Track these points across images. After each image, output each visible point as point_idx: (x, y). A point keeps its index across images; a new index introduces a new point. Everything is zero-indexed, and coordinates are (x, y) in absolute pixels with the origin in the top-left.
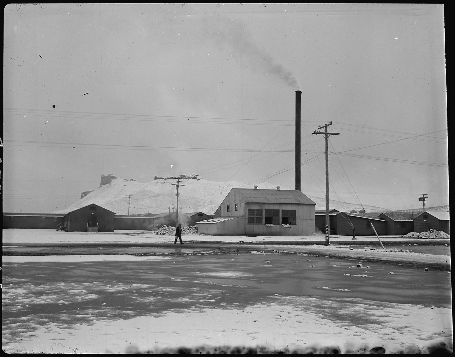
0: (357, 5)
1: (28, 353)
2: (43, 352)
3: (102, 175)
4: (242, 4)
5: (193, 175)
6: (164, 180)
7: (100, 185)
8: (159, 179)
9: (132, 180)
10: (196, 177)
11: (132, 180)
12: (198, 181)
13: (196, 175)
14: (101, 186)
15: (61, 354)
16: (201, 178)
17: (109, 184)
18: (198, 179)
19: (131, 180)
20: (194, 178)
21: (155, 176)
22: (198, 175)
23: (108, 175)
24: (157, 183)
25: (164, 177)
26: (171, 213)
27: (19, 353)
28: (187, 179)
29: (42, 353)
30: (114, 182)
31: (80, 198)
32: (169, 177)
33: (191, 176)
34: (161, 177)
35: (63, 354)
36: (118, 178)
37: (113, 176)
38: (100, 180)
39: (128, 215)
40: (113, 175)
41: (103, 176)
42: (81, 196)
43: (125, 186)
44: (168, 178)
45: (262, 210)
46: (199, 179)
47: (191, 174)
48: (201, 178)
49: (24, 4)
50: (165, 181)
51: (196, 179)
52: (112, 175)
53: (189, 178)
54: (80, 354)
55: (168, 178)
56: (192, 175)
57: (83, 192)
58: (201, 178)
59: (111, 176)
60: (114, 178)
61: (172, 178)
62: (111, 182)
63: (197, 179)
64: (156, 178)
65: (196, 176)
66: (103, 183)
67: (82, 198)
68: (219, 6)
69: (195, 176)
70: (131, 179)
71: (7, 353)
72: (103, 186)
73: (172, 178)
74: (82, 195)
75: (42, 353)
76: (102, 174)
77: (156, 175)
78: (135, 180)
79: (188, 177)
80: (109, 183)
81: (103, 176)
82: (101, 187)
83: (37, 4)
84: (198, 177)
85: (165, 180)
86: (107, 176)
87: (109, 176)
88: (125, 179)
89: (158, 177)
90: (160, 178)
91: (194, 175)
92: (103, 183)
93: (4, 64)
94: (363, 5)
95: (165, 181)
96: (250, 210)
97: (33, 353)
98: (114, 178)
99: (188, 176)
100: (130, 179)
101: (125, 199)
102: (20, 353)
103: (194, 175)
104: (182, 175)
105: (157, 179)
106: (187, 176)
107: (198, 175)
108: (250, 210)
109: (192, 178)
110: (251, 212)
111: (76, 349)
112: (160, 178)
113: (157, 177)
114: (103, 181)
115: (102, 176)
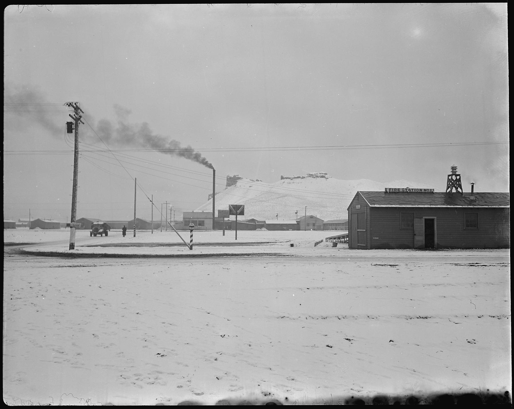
0: (408, 4)
1: (34, 405)
2: (50, 404)
3: (227, 176)
4: (277, 4)
5: (321, 173)
6: (290, 179)
7: (226, 186)
8: (285, 179)
9: (257, 180)
10: (324, 176)
11: (258, 181)
12: (326, 180)
13: (324, 174)
14: (227, 187)
15: (72, 406)
16: (330, 177)
17: (234, 186)
18: (326, 177)
19: (256, 181)
20: (322, 177)
21: (281, 176)
22: (326, 174)
23: (233, 175)
24: (283, 183)
25: (290, 177)
26: (154, 222)
27: (23, 405)
28: (315, 178)
29: (50, 404)
30: (239, 183)
31: (208, 200)
32: (296, 176)
33: (319, 175)
34: (287, 177)
35: (74, 406)
36: (244, 179)
37: (238, 176)
38: (225, 182)
39: (212, 219)
40: (238, 175)
41: (228, 177)
42: (208, 198)
43: (250, 187)
44: (295, 178)
45: (190, 221)
46: (328, 177)
47: (319, 173)
48: (329, 176)
49: (27, 5)
50: (292, 181)
51: (324, 178)
52: (237, 176)
53: (318, 177)
54: (93, 406)
55: (295, 178)
56: (321, 174)
57: (210, 194)
58: (330, 177)
59: (237, 177)
60: (239, 178)
61: (299, 177)
62: (236, 184)
63: (325, 178)
64: (282, 178)
65: (324, 175)
66: (228, 185)
67: (209, 200)
68: (250, 6)
69: (323, 174)
70: (257, 180)
71: (10, 405)
72: (229, 187)
73: (299, 177)
74: (209, 197)
75: (50, 404)
76: (228, 175)
77: (282, 175)
78: (261, 181)
79: (316, 176)
80: (234, 184)
81: (228, 177)
82: (227, 188)
83: (42, 5)
84: (326, 176)
85: (291, 180)
86: (232, 177)
87: (235, 176)
88: (251, 179)
89: (284, 177)
90: (287, 178)
91: (322, 174)
92: (228, 185)
93: (5, 74)
94: (416, 5)
95: (291, 181)
96: (185, 221)
97: (38, 405)
98: (239, 178)
99: (316, 174)
100: (256, 180)
101: (250, 201)
102: (25, 405)
103: (322, 174)
104: (309, 174)
105: (284, 179)
106: (315, 175)
107: (326, 174)
108: (185, 221)
109: (320, 177)
110: (185, 221)
111: (89, 400)
112: (287, 178)
113: (284, 176)
114: (229, 182)
115: (227, 177)
